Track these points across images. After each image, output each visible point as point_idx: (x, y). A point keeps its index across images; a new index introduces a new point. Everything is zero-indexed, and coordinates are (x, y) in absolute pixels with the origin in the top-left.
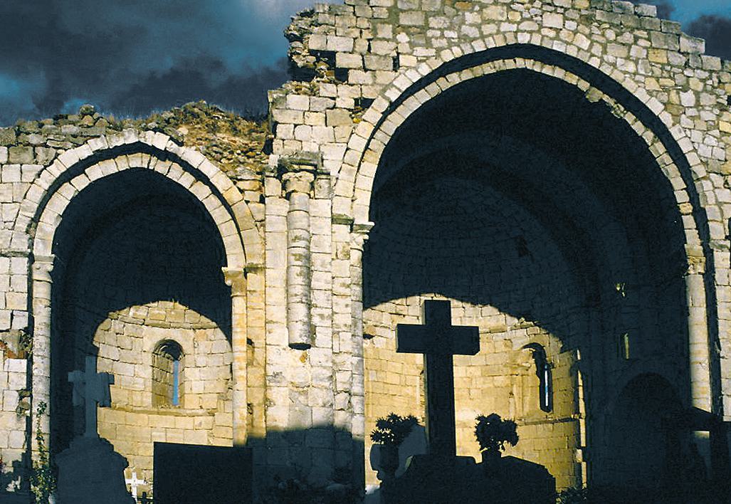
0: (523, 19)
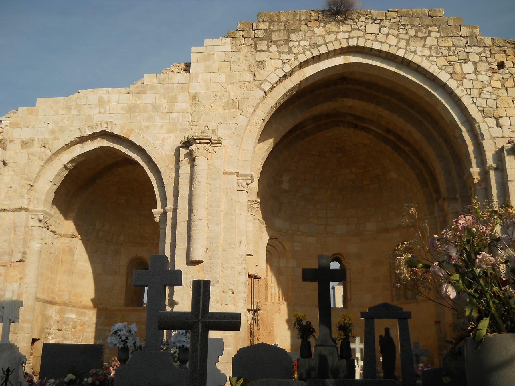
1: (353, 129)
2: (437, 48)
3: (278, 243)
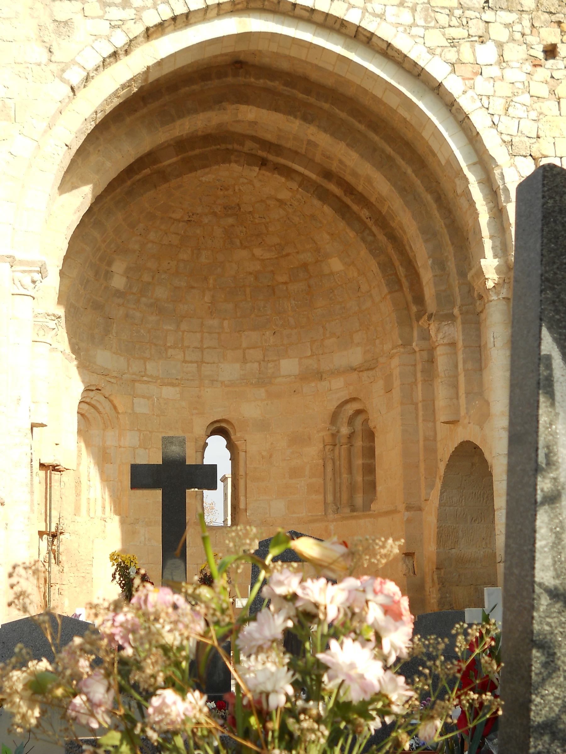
1: (257, 169)
2: (427, 10)
3: (102, 399)
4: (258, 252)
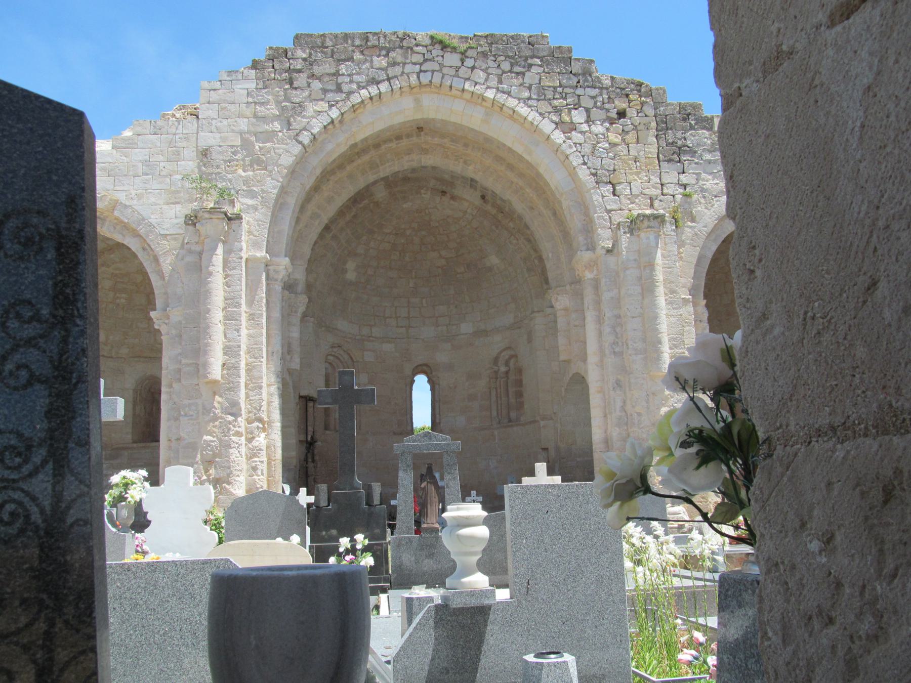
0: (426, 60)
3: (341, 352)
4: (443, 253)
